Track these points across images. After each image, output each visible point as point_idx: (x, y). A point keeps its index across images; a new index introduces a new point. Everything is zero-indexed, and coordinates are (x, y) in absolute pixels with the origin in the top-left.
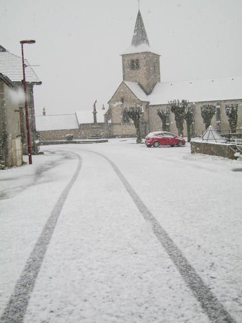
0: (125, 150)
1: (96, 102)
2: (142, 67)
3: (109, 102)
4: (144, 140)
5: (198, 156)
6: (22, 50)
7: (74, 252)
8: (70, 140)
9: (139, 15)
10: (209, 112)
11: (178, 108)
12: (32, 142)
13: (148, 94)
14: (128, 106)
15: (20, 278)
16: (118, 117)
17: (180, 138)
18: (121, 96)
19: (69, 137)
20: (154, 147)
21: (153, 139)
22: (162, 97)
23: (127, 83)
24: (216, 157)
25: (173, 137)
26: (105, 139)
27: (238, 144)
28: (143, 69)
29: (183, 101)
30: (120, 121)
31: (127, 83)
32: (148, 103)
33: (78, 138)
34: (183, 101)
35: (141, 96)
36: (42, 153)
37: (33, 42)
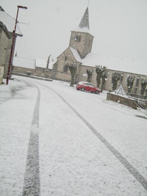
0: (62, 88)
1: (50, 56)
2: (82, 41)
3: (58, 58)
4: (75, 86)
5: (111, 102)
6: (17, 14)
7: (60, 156)
8: (29, 75)
9: (87, 10)
10: (117, 78)
11: (100, 70)
12: (10, 71)
13: (82, 57)
14: (69, 62)
15: (26, 171)
16: (61, 68)
17: (98, 89)
18: (66, 56)
19: (28, 73)
20: (81, 91)
21: (82, 86)
22: (90, 62)
23: (71, 48)
24: (124, 105)
25: (94, 87)
26: (51, 79)
27: (140, 100)
28: (82, 42)
29: (104, 67)
30: (62, 70)
31: (71, 48)
32: (81, 63)
33: (34, 75)
34: (104, 67)
35: (78, 59)
36: (13, 79)
37: (26, 8)
